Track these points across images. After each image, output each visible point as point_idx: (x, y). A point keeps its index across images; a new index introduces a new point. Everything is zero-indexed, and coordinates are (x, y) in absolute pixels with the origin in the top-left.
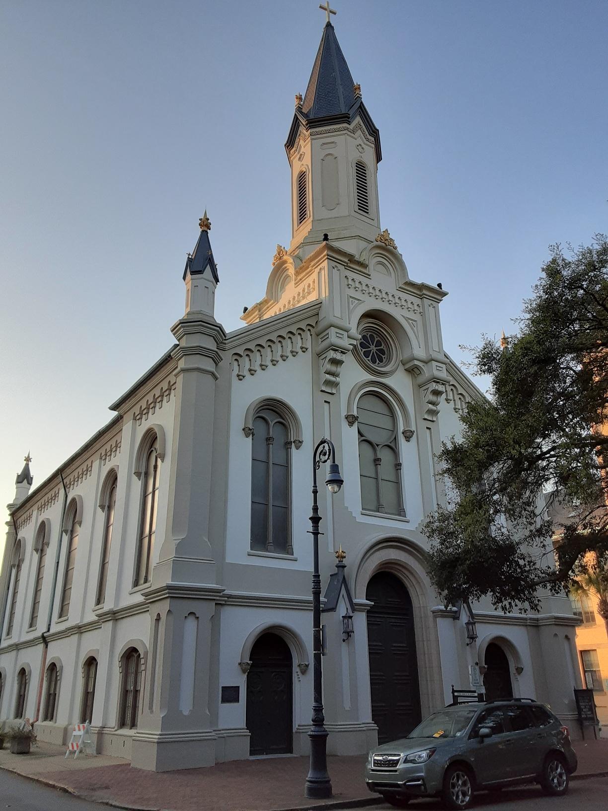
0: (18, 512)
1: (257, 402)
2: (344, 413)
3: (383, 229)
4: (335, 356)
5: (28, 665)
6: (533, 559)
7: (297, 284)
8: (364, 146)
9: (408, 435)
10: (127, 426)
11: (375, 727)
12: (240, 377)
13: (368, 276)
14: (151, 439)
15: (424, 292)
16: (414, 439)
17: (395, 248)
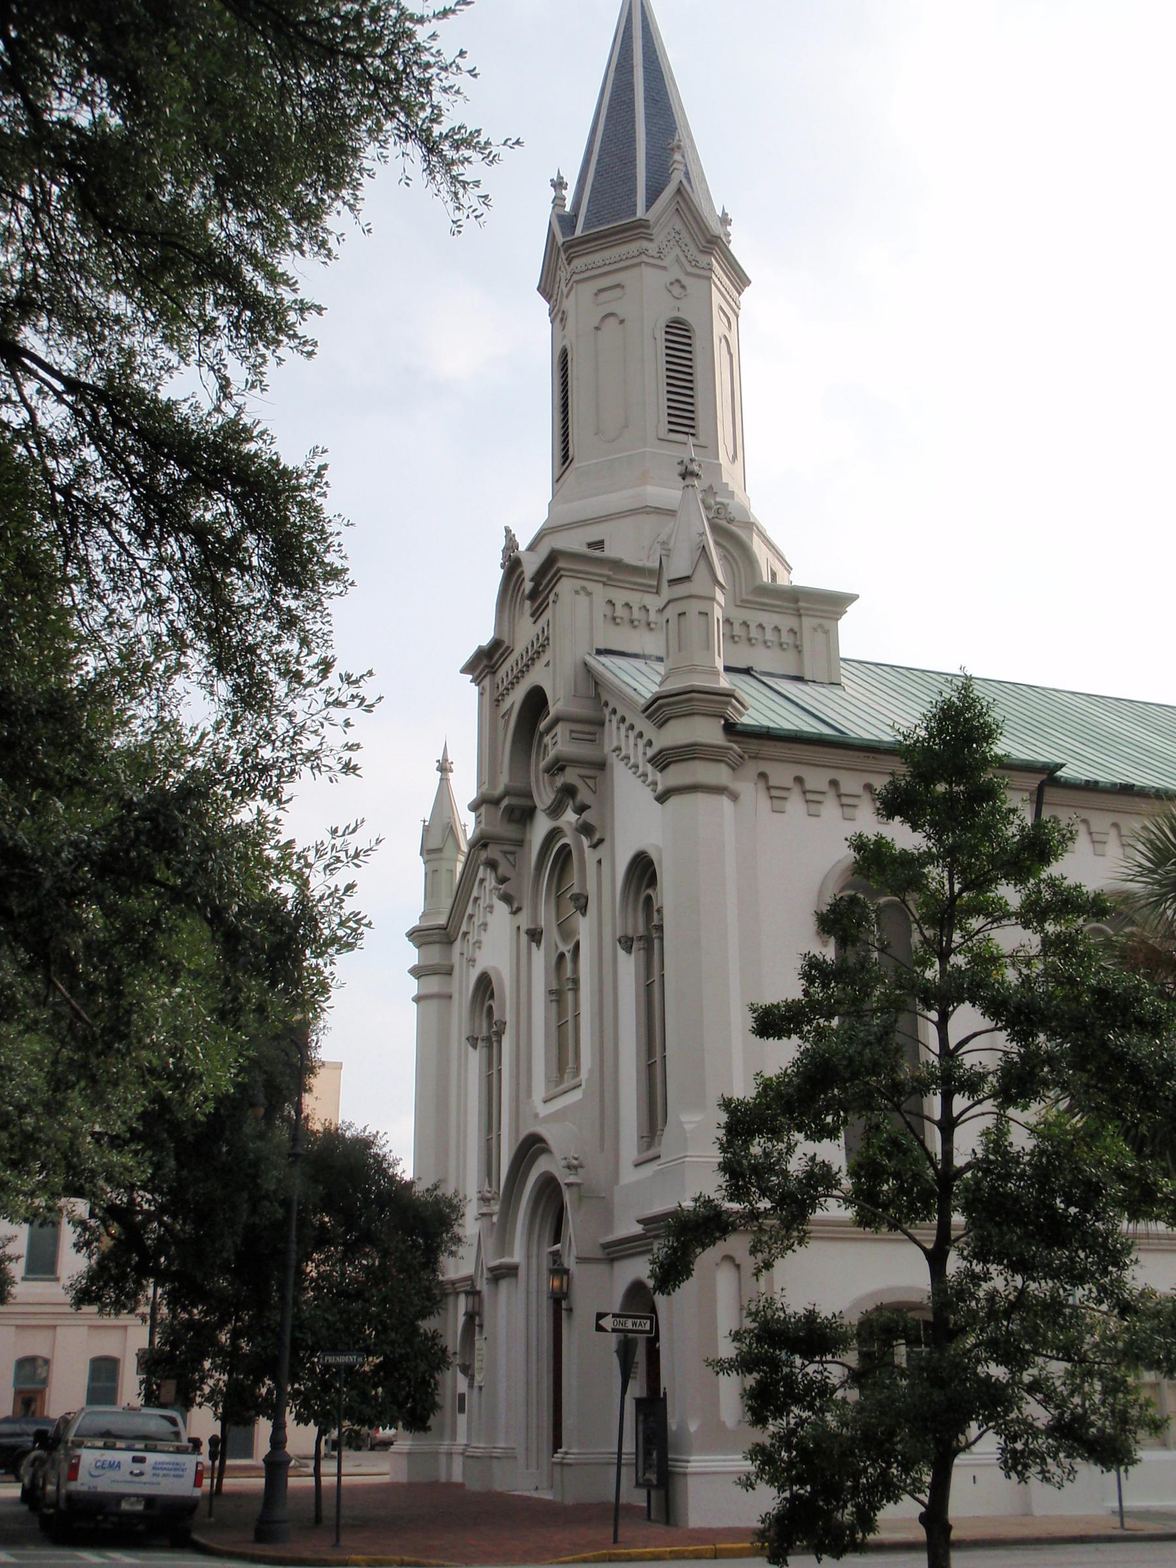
8: (686, 281)
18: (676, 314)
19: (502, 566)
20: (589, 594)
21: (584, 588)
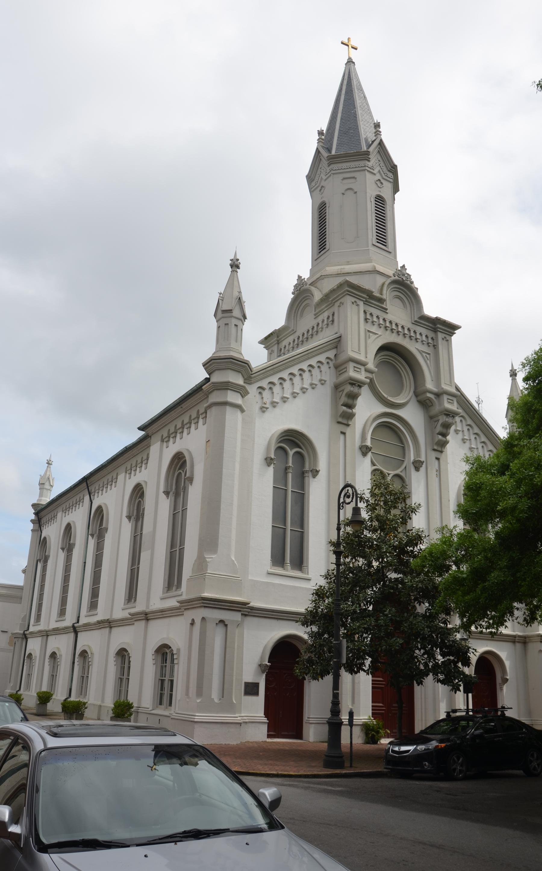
0: (42, 514)
1: (280, 432)
2: (358, 443)
3: (400, 265)
5: (58, 649)
7: (316, 316)
8: (382, 181)
9: (417, 465)
10: (155, 448)
11: (265, 720)
12: (263, 409)
13: (385, 310)
14: (179, 461)
15: (438, 326)
17: (412, 283)
18: (379, 193)
19: (293, 293)
20: (358, 305)
21: (355, 302)
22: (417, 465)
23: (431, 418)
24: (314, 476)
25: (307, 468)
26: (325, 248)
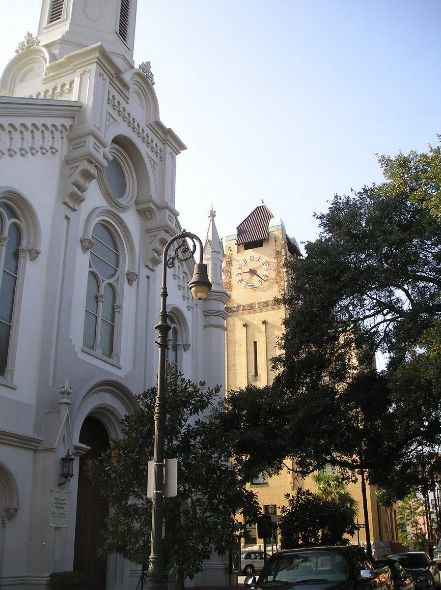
2: (80, 236)
4: (89, 168)
6: (414, 151)
13: (126, 99)
15: (169, 138)
16: (135, 283)
22: (131, 277)
23: (148, 231)
24: (33, 259)
25: (24, 245)
26: (60, 18)
